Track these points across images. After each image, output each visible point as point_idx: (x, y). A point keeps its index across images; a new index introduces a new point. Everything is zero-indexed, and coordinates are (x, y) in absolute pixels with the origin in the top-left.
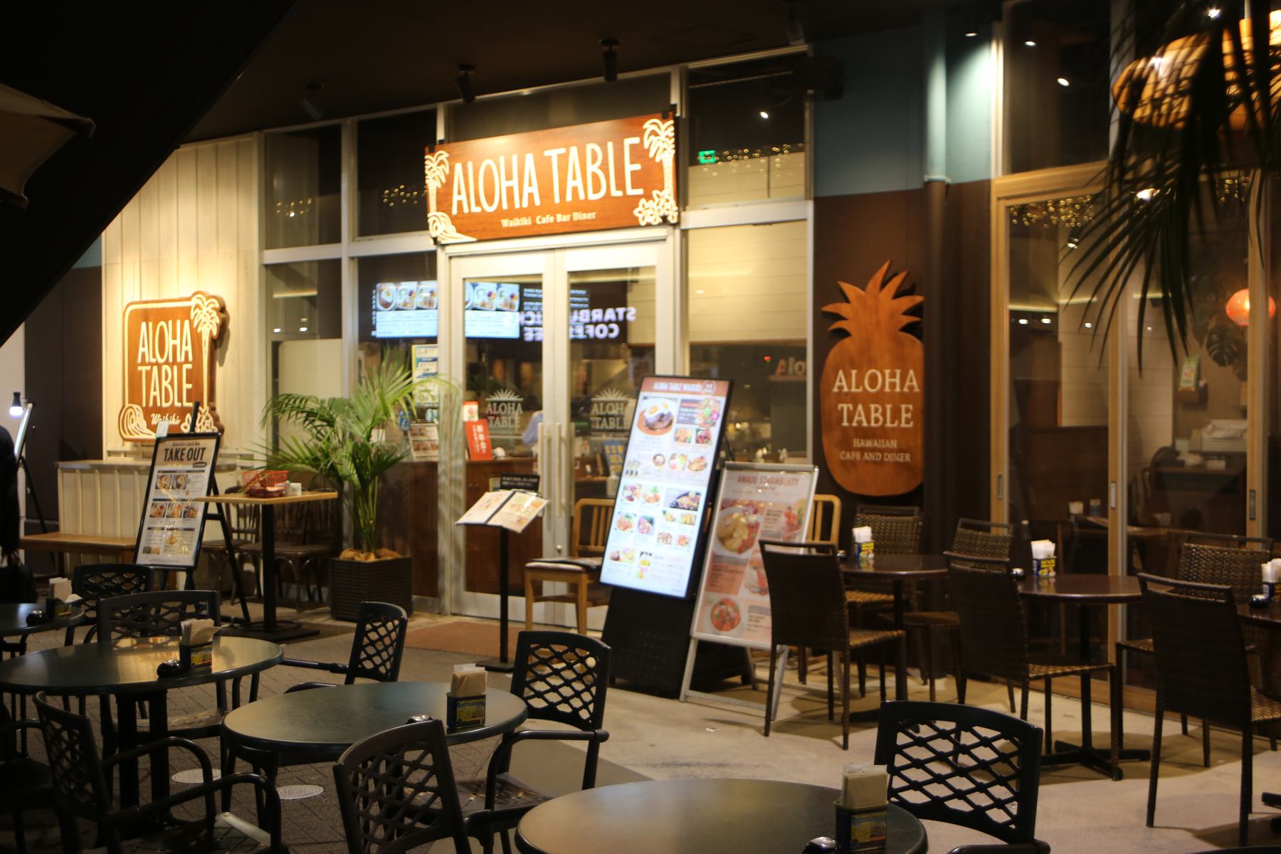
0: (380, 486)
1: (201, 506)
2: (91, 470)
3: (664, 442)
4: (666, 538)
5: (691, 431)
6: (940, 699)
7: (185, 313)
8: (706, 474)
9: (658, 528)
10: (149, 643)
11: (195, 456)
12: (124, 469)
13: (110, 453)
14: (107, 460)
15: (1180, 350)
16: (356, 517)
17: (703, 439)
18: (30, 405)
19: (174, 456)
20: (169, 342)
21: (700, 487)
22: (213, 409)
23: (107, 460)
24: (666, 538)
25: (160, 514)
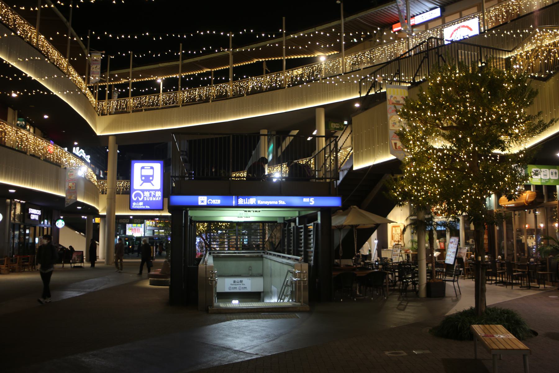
0: (269, 236)
1: (399, 254)
2: (386, 250)
3: (452, 245)
4: (452, 257)
5: (455, 243)
6: (431, 266)
7: (399, 226)
8: (456, 249)
9: (451, 256)
10: (130, 53)
11: (398, 247)
12: (390, 250)
13: (390, 248)
14: (389, 249)
15: (546, 231)
16: (142, 206)
17: (456, 244)
18: (527, 204)
19: (396, 248)
20: (397, 230)
21: (455, 250)
22: (403, 241)
23: (389, 249)
24: (452, 257)
25: (394, 255)
